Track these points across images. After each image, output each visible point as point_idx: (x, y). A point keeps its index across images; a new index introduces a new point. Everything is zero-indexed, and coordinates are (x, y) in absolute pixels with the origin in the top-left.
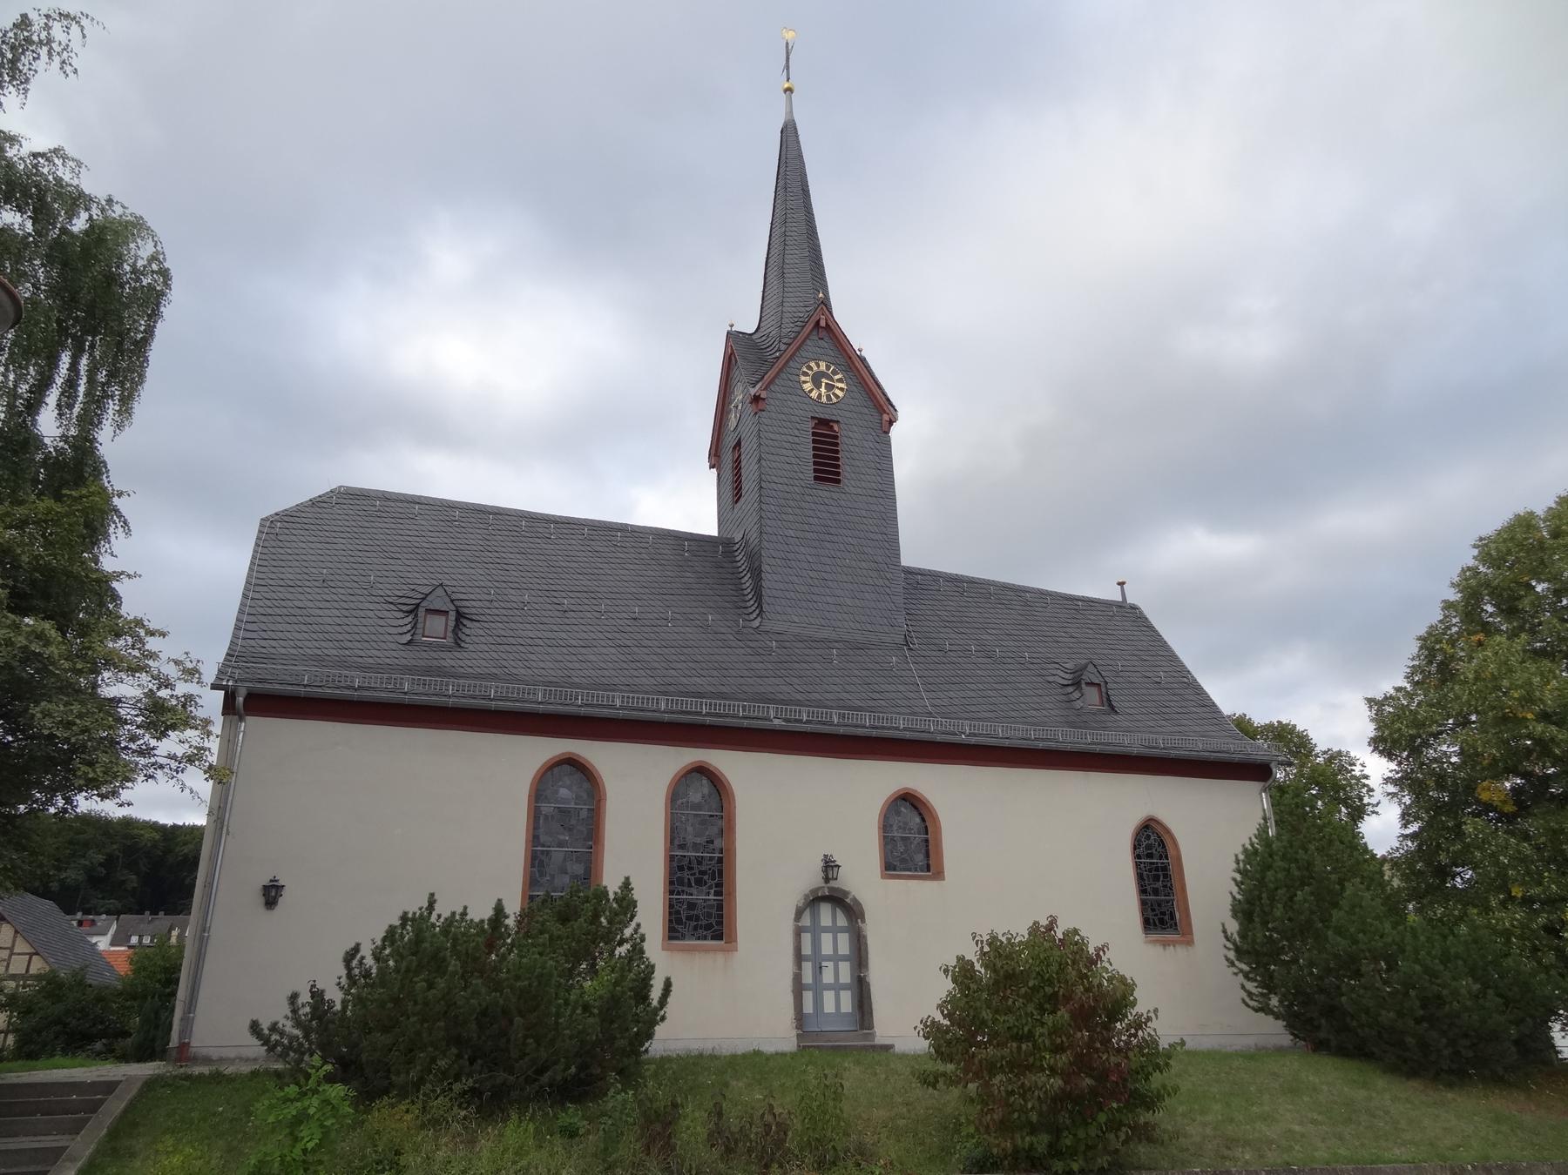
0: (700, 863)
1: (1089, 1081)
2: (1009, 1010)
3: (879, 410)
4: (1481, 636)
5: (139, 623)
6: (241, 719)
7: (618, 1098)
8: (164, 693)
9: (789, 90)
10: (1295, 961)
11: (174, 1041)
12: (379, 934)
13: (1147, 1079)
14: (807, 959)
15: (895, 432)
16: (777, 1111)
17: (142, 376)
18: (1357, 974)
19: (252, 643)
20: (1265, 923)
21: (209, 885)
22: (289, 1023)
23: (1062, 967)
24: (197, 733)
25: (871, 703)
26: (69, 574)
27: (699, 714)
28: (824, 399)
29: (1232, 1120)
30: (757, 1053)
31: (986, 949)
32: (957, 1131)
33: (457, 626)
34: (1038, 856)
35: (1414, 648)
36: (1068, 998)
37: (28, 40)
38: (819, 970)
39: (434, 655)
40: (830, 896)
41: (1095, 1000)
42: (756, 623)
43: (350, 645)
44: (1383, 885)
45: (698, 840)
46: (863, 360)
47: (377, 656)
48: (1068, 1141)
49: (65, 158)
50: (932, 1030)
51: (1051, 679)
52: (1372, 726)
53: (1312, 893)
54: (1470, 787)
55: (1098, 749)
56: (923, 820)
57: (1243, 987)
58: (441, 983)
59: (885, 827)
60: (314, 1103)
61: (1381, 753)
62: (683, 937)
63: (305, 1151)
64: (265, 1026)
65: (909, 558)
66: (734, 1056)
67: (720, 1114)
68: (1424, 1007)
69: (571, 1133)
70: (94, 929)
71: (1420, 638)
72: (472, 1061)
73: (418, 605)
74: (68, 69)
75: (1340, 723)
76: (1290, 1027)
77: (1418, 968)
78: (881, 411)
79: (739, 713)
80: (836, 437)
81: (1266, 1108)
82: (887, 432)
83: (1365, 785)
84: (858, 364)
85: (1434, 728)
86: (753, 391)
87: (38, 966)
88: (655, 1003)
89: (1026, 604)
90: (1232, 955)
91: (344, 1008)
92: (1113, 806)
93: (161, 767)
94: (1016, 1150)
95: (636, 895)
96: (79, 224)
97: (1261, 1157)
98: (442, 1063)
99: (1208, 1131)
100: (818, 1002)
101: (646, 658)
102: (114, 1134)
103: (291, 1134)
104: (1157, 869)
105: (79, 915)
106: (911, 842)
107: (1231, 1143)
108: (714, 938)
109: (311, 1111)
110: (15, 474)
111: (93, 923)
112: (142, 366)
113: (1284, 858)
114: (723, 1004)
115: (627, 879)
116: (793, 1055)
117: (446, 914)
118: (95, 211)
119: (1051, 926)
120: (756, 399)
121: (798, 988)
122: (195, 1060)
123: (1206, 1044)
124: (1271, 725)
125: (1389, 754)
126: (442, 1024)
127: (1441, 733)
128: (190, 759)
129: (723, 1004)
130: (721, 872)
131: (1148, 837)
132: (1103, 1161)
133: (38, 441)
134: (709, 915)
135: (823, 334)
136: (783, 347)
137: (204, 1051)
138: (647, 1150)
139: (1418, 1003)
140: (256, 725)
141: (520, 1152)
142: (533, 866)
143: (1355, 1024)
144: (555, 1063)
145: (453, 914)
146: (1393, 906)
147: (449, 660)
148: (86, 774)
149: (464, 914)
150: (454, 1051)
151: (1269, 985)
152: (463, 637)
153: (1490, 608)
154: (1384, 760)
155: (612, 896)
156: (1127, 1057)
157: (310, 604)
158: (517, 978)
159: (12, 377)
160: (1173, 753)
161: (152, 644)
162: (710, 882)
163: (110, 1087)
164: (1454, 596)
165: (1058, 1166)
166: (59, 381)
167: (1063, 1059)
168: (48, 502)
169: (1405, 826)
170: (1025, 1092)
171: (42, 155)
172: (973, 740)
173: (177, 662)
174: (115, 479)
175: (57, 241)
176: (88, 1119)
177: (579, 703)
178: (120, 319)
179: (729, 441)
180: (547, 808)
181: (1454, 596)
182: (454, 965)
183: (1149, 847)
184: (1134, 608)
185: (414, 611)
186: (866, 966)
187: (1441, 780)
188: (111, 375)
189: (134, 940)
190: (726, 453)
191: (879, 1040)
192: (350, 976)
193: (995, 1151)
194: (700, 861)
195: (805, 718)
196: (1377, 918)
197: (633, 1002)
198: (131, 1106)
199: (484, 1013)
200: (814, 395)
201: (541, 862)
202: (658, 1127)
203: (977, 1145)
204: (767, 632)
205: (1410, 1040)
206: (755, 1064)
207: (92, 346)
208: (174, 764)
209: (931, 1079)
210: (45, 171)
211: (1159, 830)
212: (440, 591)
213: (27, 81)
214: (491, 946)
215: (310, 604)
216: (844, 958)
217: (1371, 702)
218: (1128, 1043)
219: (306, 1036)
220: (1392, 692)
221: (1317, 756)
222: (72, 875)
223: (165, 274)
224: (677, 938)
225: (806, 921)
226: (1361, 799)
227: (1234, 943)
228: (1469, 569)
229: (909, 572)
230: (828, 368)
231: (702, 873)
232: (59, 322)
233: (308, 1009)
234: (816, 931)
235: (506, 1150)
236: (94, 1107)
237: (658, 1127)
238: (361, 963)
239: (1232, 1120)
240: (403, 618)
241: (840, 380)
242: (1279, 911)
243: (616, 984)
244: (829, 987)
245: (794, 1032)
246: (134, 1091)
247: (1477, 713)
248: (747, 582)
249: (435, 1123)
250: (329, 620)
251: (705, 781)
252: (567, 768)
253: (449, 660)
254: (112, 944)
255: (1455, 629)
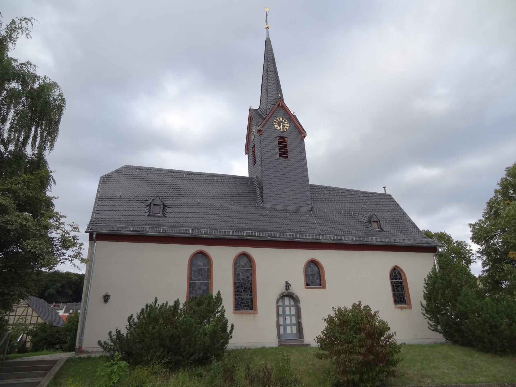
0: (244, 285)
1: (372, 357)
2: (345, 333)
3: (300, 133)
4: (508, 202)
5: (57, 213)
6: (95, 242)
7: (216, 364)
8: (67, 235)
9: (267, 28)
10: (446, 314)
11: (77, 346)
12: (139, 311)
13: (392, 356)
14: (281, 316)
15: (306, 140)
16: (268, 368)
17: (57, 133)
18: (467, 318)
19: (98, 217)
20: (435, 301)
21: (86, 295)
22: (110, 341)
23: (362, 318)
24: (77, 248)
25: (300, 230)
26: (36, 199)
27: (243, 236)
28: (282, 130)
29: (423, 369)
30: (264, 348)
31: (337, 313)
32: (329, 374)
33: (163, 209)
34: (357, 281)
35: (485, 206)
36: (364, 329)
37: (15, 28)
38: (285, 319)
39: (156, 219)
40: (288, 295)
41: (374, 330)
42: (261, 205)
43: (129, 217)
44: (476, 286)
45: (244, 277)
46: (294, 116)
47: (138, 220)
48: (366, 377)
49: (31, 65)
50: (320, 340)
51: (361, 220)
52: (472, 233)
53: (451, 291)
54: (506, 253)
55: (377, 243)
56: (319, 269)
57: (428, 323)
58: (157, 327)
59: (306, 271)
60: (115, 368)
61: (475, 242)
62: (240, 309)
63: (114, 383)
64: (103, 342)
65: (312, 181)
66: (256, 349)
67: (249, 369)
68: (491, 329)
69: (200, 376)
70: (59, 308)
71: (487, 203)
72: (168, 353)
73: (151, 203)
74: (28, 36)
75: (460, 231)
76: (445, 336)
77: (488, 315)
78: (301, 133)
79: (256, 235)
80: (286, 142)
81: (436, 364)
82: (303, 140)
83: (471, 253)
84: (293, 118)
85: (493, 234)
86: (258, 128)
87: (40, 321)
88: (229, 332)
89: (352, 195)
90: (424, 312)
91: (127, 336)
92: (384, 262)
93: (66, 259)
94: (348, 380)
95: (222, 297)
96: (36, 86)
97: (434, 381)
98: (158, 354)
99: (415, 373)
100: (285, 330)
101: (225, 218)
102: (55, 378)
103: (109, 377)
104: (398, 283)
105: (54, 304)
106: (315, 276)
107: (423, 376)
108: (250, 309)
109: (115, 370)
110: (19, 167)
111: (58, 306)
112: (57, 130)
113: (441, 278)
114: (252, 332)
115: (219, 291)
116: (276, 348)
117: (161, 304)
118: (41, 81)
119: (360, 304)
120: (259, 131)
121: (278, 325)
122: (83, 352)
123: (417, 342)
124: (438, 233)
125: (478, 243)
126: (158, 340)
127: (495, 235)
128: (75, 257)
129: (252, 332)
130: (251, 288)
131: (395, 273)
132: (378, 384)
133: (26, 156)
134: (248, 302)
135: (281, 108)
136: (268, 113)
137: (87, 349)
138: (225, 381)
139: (488, 327)
140: (100, 244)
141: (183, 383)
142: (190, 287)
143: (467, 335)
144: (196, 353)
145: (163, 304)
146: (480, 295)
147: (161, 221)
148: (41, 263)
149: (167, 304)
150: (162, 349)
151: (437, 322)
152: (166, 213)
153: (511, 192)
154: (476, 245)
155: (214, 297)
156: (385, 349)
157: (116, 204)
158: (182, 325)
159: (17, 135)
160: (403, 244)
161: (62, 220)
162: (248, 291)
163: (55, 362)
164: (498, 188)
165: (362, 385)
166: (32, 136)
167: (363, 350)
168: (29, 176)
169: (484, 267)
170: (350, 361)
171: (24, 64)
172: (334, 242)
173: (71, 225)
174: (51, 167)
175: (29, 91)
176: (47, 373)
177: (203, 234)
178: (50, 115)
179: (251, 145)
180: (194, 268)
181: (498, 188)
182: (161, 321)
183: (396, 276)
184: (389, 195)
185: (149, 205)
186: (301, 318)
187: (496, 251)
188: (48, 133)
189: (71, 311)
190: (250, 149)
191: (306, 342)
192: (130, 325)
193: (341, 381)
194: (244, 284)
195: (278, 236)
196: (474, 299)
197: (221, 332)
198: (61, 369)
199: (172, 336)
200: (278, 129)
201: (193, 287)
202: (228, 374)
203: (336, 378)
204: (265, 208)
205: (486, 340)
206: (263, 352)
207: (42, 124)
208: (70, 259)
209: (320, 356)
210: (25, 69)
211: (399, 269)
212: (158, 198)
213: (15, 41)
214: (174, 315)
215: (116, 204)
216: (293, 315)
217: (471, 225)
218: (386, 344)
219: (115, 345)
220: (478, 221)
221: (454, 243)
222: (52, 291)
223: (63, 100)
224: (238, 310)
225: (280, 303)
226: (469, 257)
227: (425, 308)
228: (504, 178)
229: (312, 186)
230: (283, 119)
231: (245, 288)
232: (31, 117)
233: (115, 337)
234: (284, 306)
235: (179, 382)
236: (50, 368)
237: (228, 374)
238: (133, 321)
239: (423, 369)
240: (147, 208)
241: (287, 124)
242: (439, 297)
243: (215, 326)
244: (288, 325)
245: (277, 340)
246: (63, 363)
247: (507, 227)
248: (258, 192)
249: (156, 373)
250: (122, 209)
251: (245, 258)
252: (200, 255)
253: (161, 221)
254: (64, 313)
255: (499, 199)
